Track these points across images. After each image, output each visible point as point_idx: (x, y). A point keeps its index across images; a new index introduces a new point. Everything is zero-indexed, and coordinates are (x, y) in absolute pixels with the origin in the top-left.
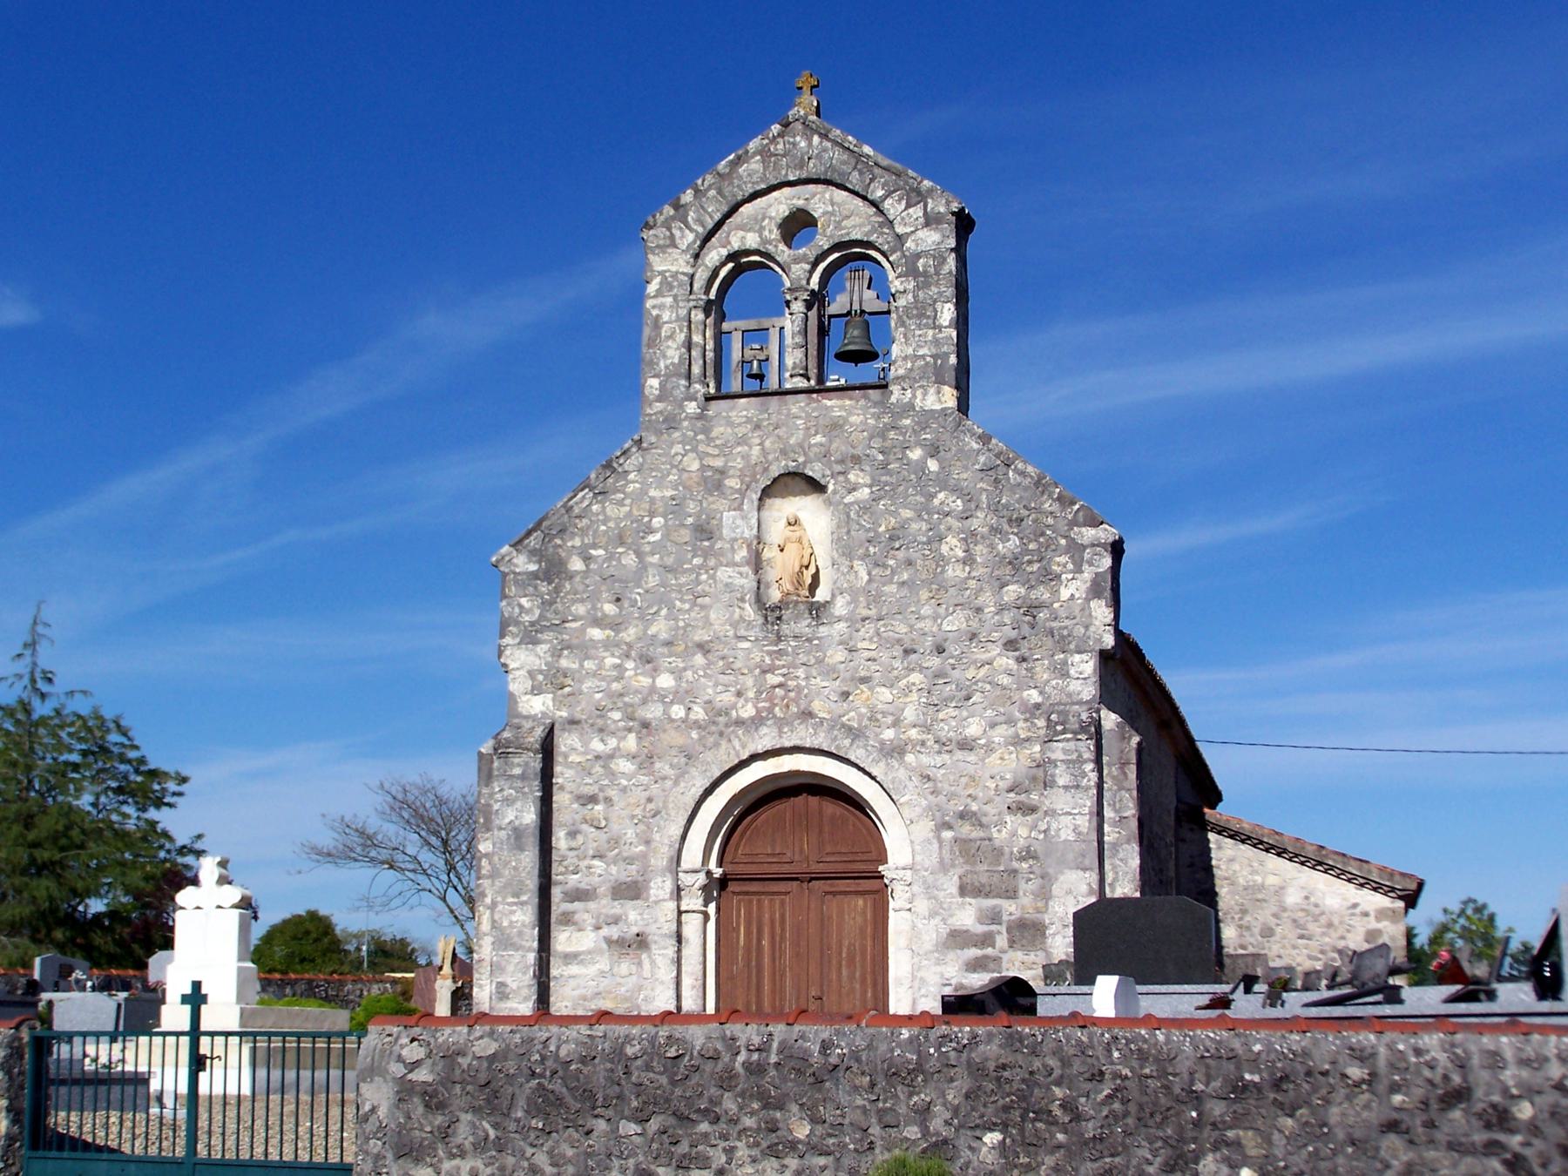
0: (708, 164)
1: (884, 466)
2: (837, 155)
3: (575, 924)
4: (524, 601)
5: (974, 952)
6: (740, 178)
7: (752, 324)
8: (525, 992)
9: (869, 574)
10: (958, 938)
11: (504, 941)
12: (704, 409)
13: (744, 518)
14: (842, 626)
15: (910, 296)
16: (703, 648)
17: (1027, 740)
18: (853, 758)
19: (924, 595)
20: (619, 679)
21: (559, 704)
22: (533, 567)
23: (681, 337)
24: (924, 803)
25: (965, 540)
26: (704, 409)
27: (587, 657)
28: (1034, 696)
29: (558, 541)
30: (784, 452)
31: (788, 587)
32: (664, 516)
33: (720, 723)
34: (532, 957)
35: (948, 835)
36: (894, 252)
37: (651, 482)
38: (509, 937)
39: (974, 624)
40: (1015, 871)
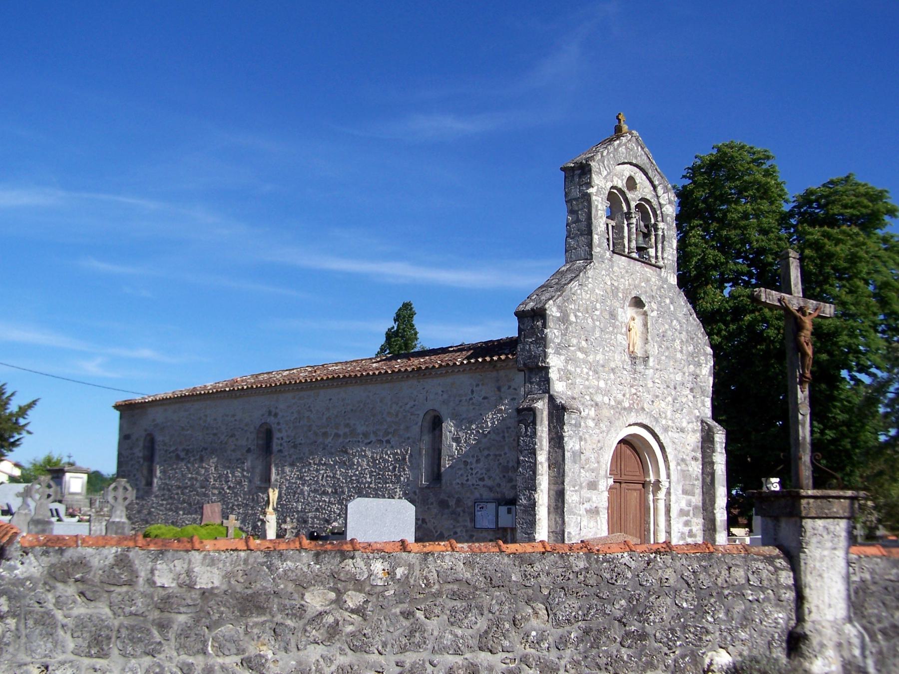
35: (679, 468)
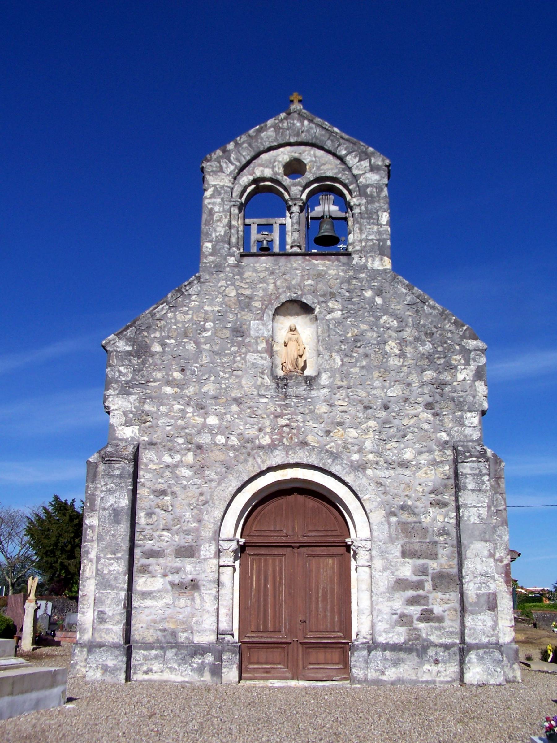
0: (244, 130)
1: (350, 299)
2: (318, 131)
3: (149, 572)
4: (122, 369)
5: (411, 593)
6: (262, 139)
7: (263, 221)
8: (118, 618)
9: (342, 361)
10: (401, 584)
11: (104, 583)
12: (239, 261)
13: (264, 325)
14: (325, 391)
15: (363, 208)
16: (238, 401)
17: (441, 462)
18: (333, 471)
19: (376, 374)
20: (182, 418)
21: (142, 432)
22: (129, 348)
23: (226, 221)
24: (379, 499)
25: (400, 343)
26: (239, 261)
27: (162, 404)
28: (444, 436)
29: (146, 334)
30: (289, 288)
31: (289, 367)
32: (214, 322)
33: (249, 448)
34: (123, 594)
35: (394, 519)
36: (351, 184)
37: (202, 304)
38: (108, 581)
39: (407, 393)
40: (436, 542)
